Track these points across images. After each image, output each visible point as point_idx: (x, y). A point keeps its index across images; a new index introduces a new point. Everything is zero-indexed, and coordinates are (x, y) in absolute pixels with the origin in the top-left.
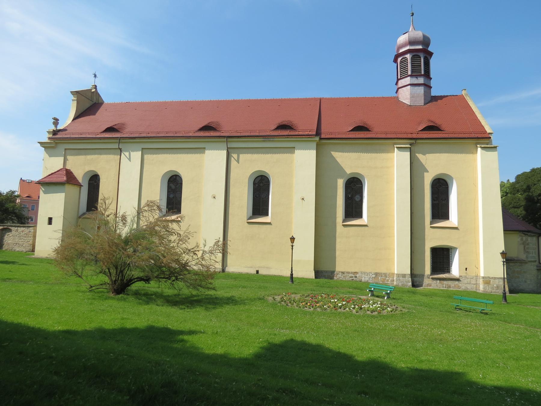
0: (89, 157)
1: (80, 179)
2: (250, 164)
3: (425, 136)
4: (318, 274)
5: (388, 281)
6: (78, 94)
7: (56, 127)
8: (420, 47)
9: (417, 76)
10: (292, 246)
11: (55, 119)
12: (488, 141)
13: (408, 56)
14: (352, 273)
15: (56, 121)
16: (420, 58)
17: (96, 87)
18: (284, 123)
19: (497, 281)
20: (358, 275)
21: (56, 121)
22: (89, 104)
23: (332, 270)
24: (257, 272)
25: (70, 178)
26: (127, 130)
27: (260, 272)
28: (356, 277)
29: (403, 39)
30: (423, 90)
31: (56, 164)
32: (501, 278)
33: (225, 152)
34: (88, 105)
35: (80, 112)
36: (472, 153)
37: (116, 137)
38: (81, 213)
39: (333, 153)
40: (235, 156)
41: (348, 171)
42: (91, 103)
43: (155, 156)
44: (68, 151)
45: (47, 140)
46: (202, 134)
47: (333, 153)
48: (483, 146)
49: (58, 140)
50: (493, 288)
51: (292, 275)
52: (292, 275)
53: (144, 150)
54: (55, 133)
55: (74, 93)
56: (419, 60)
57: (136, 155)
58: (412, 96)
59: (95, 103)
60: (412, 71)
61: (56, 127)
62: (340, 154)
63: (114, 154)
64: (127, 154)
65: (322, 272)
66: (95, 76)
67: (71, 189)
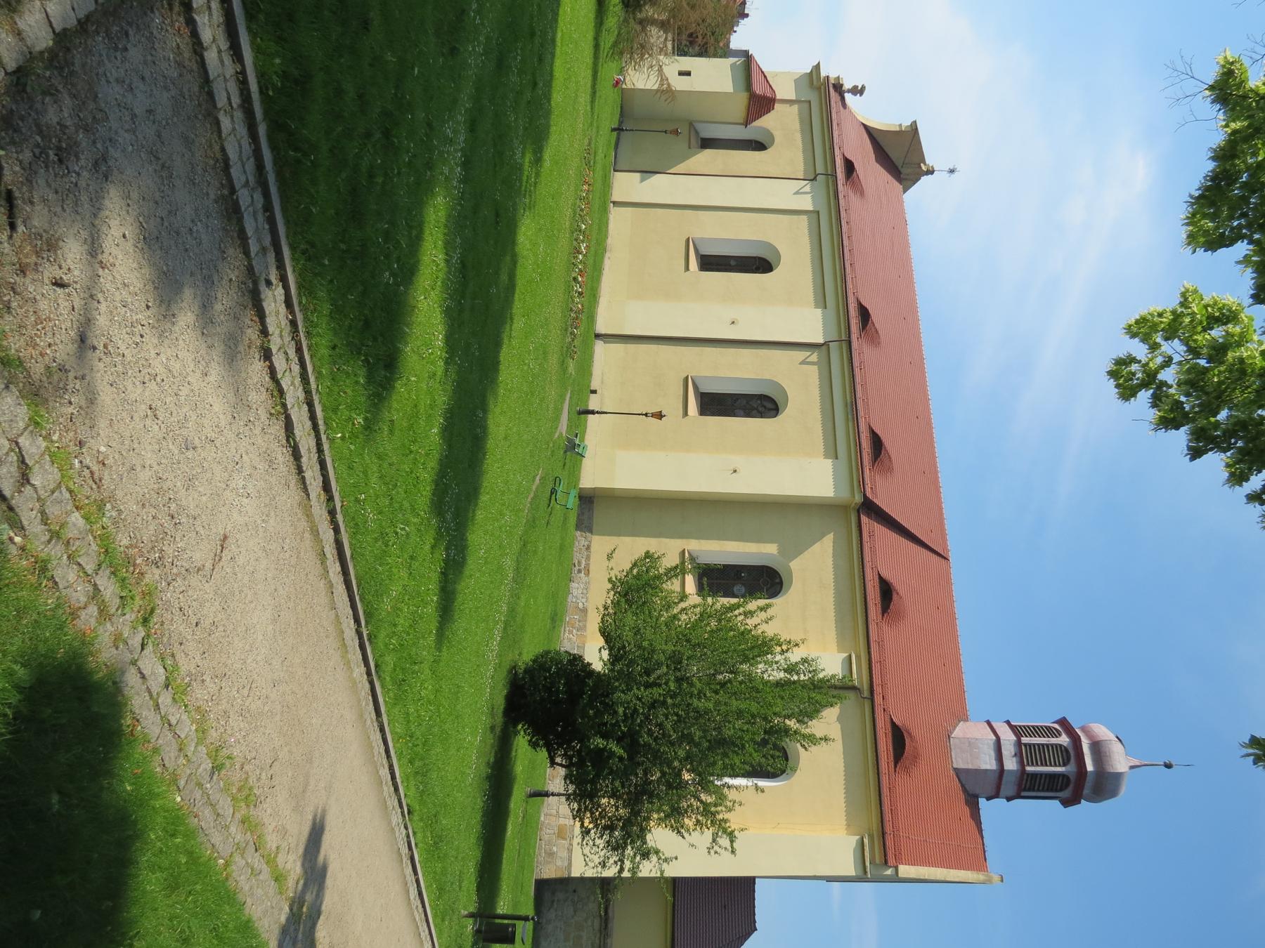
0: (798, 136)
1: (758, 123)
2: (802, 385)
3: (880, 723)
4: (588, 500)
5: (571, 632)
6: (911, 135)
7: (849, 91)
8: (1090, 767)
9: (1019, 754)
10: (646, 415)
11: (863, 88)
12: (878, 861)
13: (1064, 740)
14: (588, 565)
15: (858, 91)
16: (1064, 765)
17: (931, 172)
18: (895, 596)
19: (565, 854)
20: (582, 575)
21: (858, 91)
22: (900, 156)
23: (595, 528)
24: (594, 392)
25: (761, 104)
26: (885, 628)
27: (592, 396)
28: (579, 571)
29: (1103, 732)
30: (988, 767)
31: (784, 90)
32: (570, 872)
33: (821, 341)
34: (895, 155)
35: (879, 139)
36: (848, 825)
37: (833, 174)
38: (699, 126)
39: (831, 536)
40: (814, 357)
41: (795, 565)
42: (899, 163)
43: (806, 231)
44: (806, 105)
45: (823, 74)
46: (853, 312)
47: (831, 536)
48: (866, 841)
49: (825, 93)
50: (549, 843)
51: (593, 412)
52: (593, 412)
53: (815, 215)
54: (838, 87)
55: (914, 129)
56: (1061, 772)
57: (806, 203)
58: (971, 744)
59: (900, 173)
60: (1030, 745)
61: (849, 91)
62: (830, 551)
63: (805, 170)
64: (808, 189)
65: (591, 509)
66: (952, 171)
67: (739, 105)
